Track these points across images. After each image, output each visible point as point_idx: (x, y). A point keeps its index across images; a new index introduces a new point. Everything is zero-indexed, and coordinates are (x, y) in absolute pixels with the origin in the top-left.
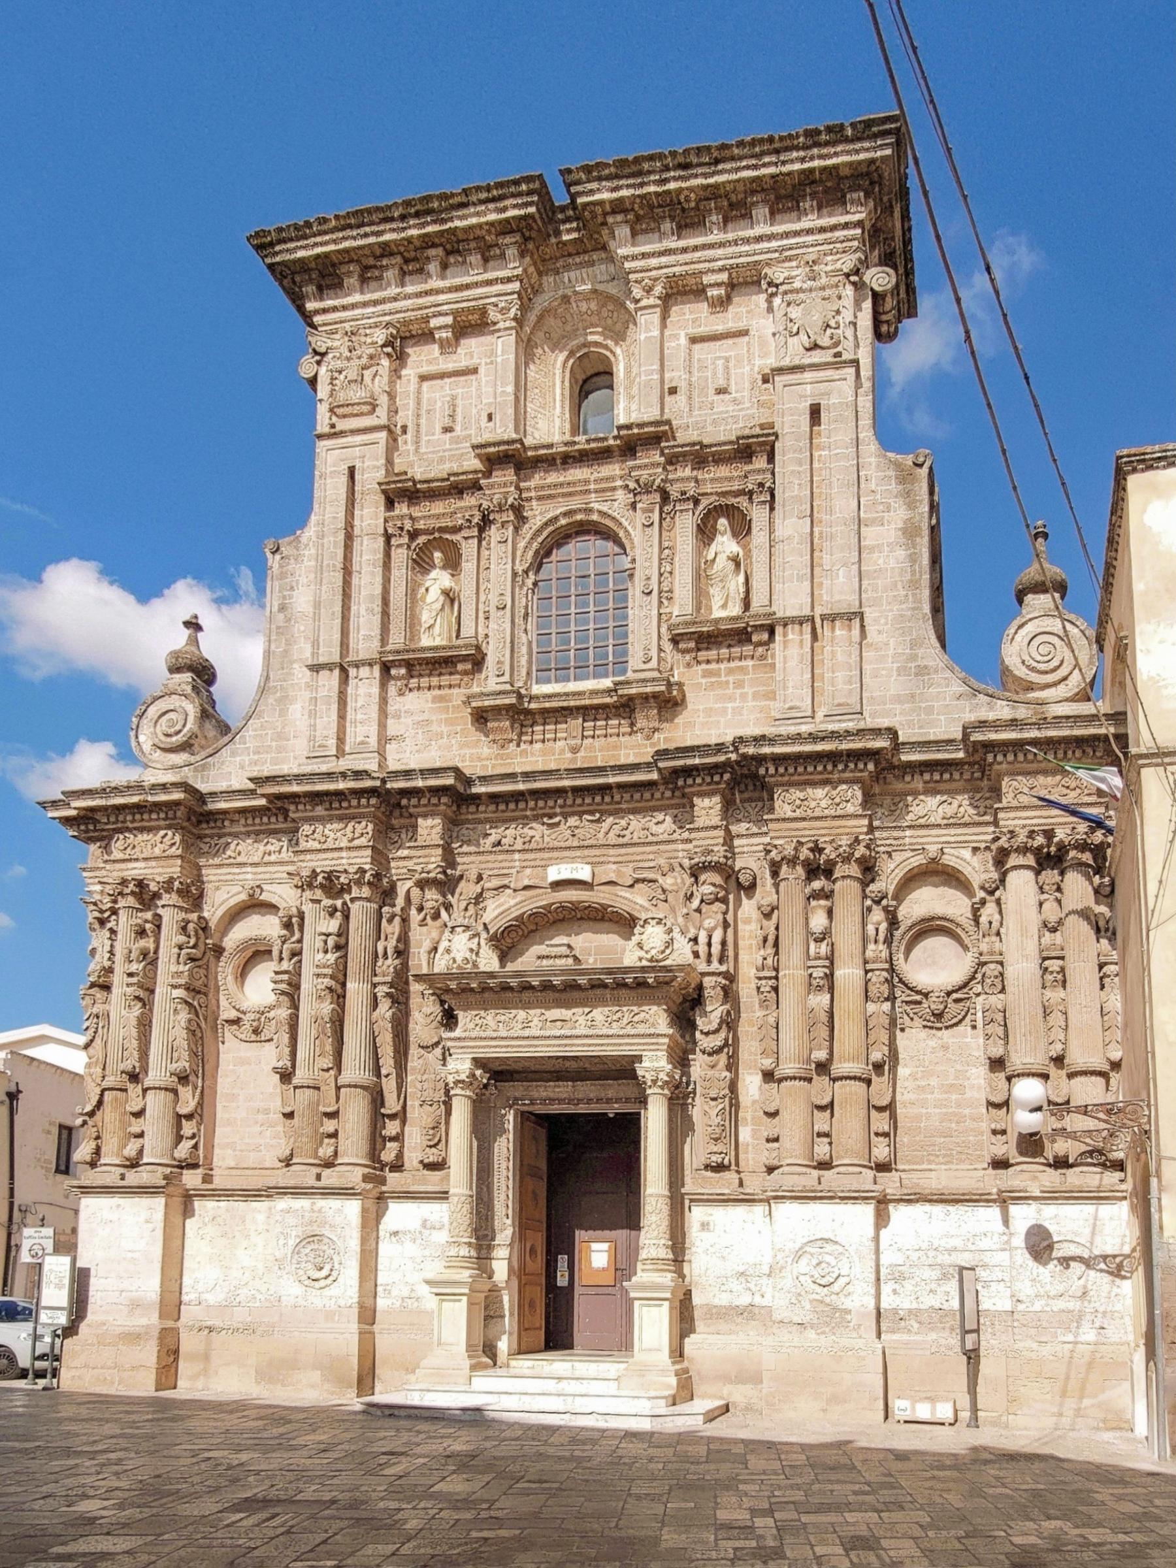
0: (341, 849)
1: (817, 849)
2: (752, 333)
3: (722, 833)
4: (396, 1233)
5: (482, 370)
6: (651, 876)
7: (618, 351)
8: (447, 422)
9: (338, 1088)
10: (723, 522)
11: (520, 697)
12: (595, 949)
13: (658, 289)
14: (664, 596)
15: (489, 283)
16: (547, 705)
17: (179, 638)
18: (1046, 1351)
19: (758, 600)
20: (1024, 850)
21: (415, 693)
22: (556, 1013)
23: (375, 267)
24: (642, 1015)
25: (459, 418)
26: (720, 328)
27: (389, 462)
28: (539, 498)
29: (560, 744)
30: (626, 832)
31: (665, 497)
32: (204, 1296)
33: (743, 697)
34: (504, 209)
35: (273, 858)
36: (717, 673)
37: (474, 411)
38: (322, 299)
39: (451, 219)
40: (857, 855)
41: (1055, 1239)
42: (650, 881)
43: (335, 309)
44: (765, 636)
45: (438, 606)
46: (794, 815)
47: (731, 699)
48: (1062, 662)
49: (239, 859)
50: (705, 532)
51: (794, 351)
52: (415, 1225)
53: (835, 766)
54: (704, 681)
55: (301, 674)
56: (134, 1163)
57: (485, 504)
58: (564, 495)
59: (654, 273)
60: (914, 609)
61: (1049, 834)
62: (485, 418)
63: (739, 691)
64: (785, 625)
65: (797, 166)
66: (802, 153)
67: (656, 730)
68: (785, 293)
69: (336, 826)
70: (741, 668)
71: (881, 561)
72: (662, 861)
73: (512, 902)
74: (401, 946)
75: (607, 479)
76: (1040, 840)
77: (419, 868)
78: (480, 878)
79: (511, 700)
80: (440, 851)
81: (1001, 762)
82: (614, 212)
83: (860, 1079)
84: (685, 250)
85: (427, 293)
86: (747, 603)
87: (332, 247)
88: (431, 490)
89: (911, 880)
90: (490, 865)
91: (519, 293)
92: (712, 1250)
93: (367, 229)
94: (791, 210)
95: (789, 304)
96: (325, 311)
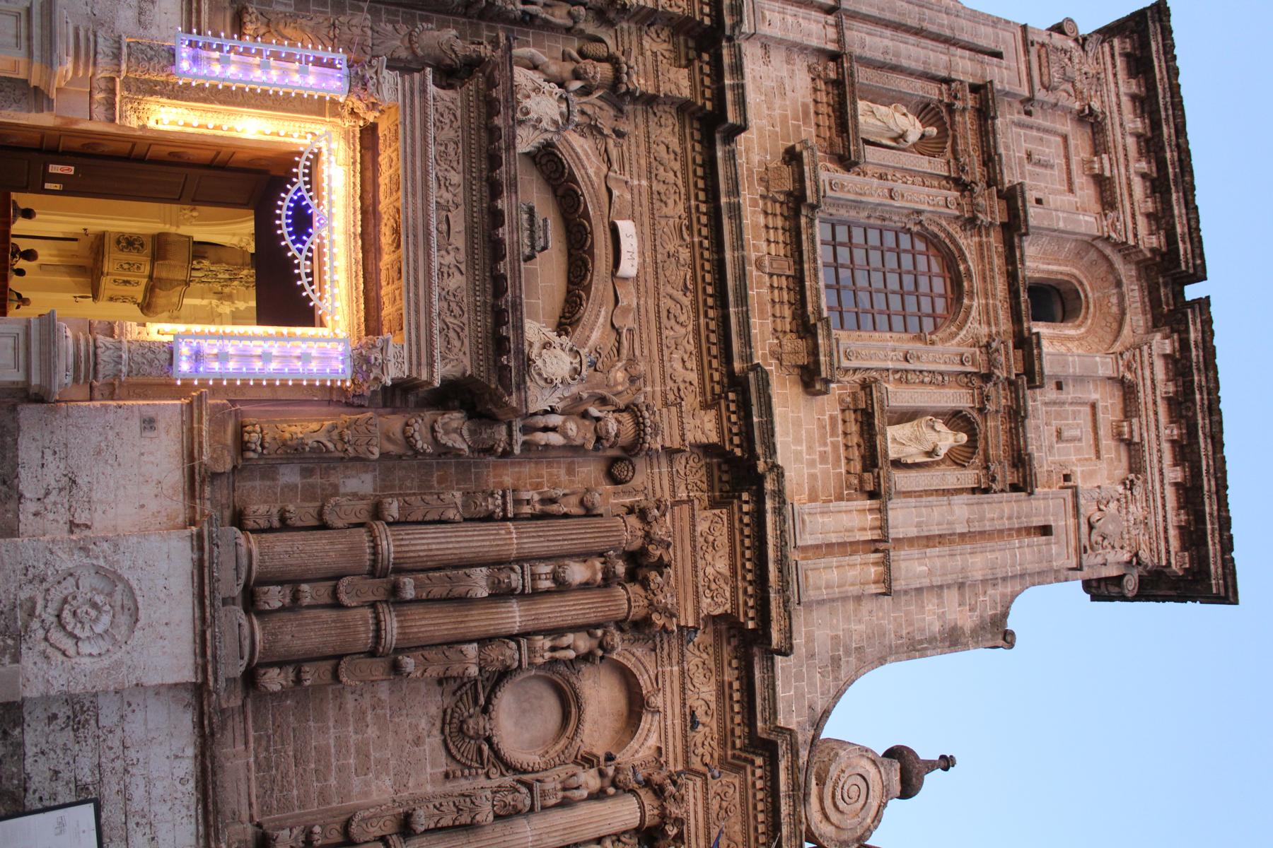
1: (660, 566)
2: (1098, 462)
3: (676, 446)
5: (1070, 197)
6: (624, 351)
7: (1083, 330)
8: (1035, 157)
11: (813, 207)
12: (544, 279)
13: (1129, 376)
14: (903, 377)
16: (804, 237)
19: (902, 480)
20: (663, 816)
21: (809, 84)
22: (458, 225)
23: (1143, 112)
24: (457, 343)
25: (1038, 170)
26: (1102, 433)
27: (1007, 94)
29: (764, 245)
30: (673, 321)
31: (986, 378)
33: (812, 463)
36: (834, 433)
37: (1043, 185)
38: (1121, 54)
39: (1177, 192)
40: (655, 617)
42: (618, 351)
43: (1114, 66)
44: (869, 487)
45: (892, 126)
46: (698, 534)
47: (810, 448)
48: (842, 812)
50: (956, 419)
51: (1088, 508)
53: (750, 583)
54: (827, 417)
57: (977, 189)
58: (984, 270)
59: (1139, 372)
60: (890, 647)
62: (1039, 195)
63: (817, 457)
64: (880, 510)
65: (1207, 509)
66: (1215, 513)
67: (780, 360)
68: (1126, 497)
70: (838, 460)
71: (930, 607)
72: (642, 367)
73: (591, 171)
74: (537, 22)
75: (996, 318)
76: (672, 831)
77: (632, 63)
78: (620, 134)
79: (811, 198)
80: (651, 91)
82: (1181, 340)
84: (1155, 403)
86: (897, 464)
87: (1158, 76)
88: (987, 133)
90: (633, 149)
91: (1126, 243)
92: (111, 435)
93: (1170, 112)
95: (1118, 500)
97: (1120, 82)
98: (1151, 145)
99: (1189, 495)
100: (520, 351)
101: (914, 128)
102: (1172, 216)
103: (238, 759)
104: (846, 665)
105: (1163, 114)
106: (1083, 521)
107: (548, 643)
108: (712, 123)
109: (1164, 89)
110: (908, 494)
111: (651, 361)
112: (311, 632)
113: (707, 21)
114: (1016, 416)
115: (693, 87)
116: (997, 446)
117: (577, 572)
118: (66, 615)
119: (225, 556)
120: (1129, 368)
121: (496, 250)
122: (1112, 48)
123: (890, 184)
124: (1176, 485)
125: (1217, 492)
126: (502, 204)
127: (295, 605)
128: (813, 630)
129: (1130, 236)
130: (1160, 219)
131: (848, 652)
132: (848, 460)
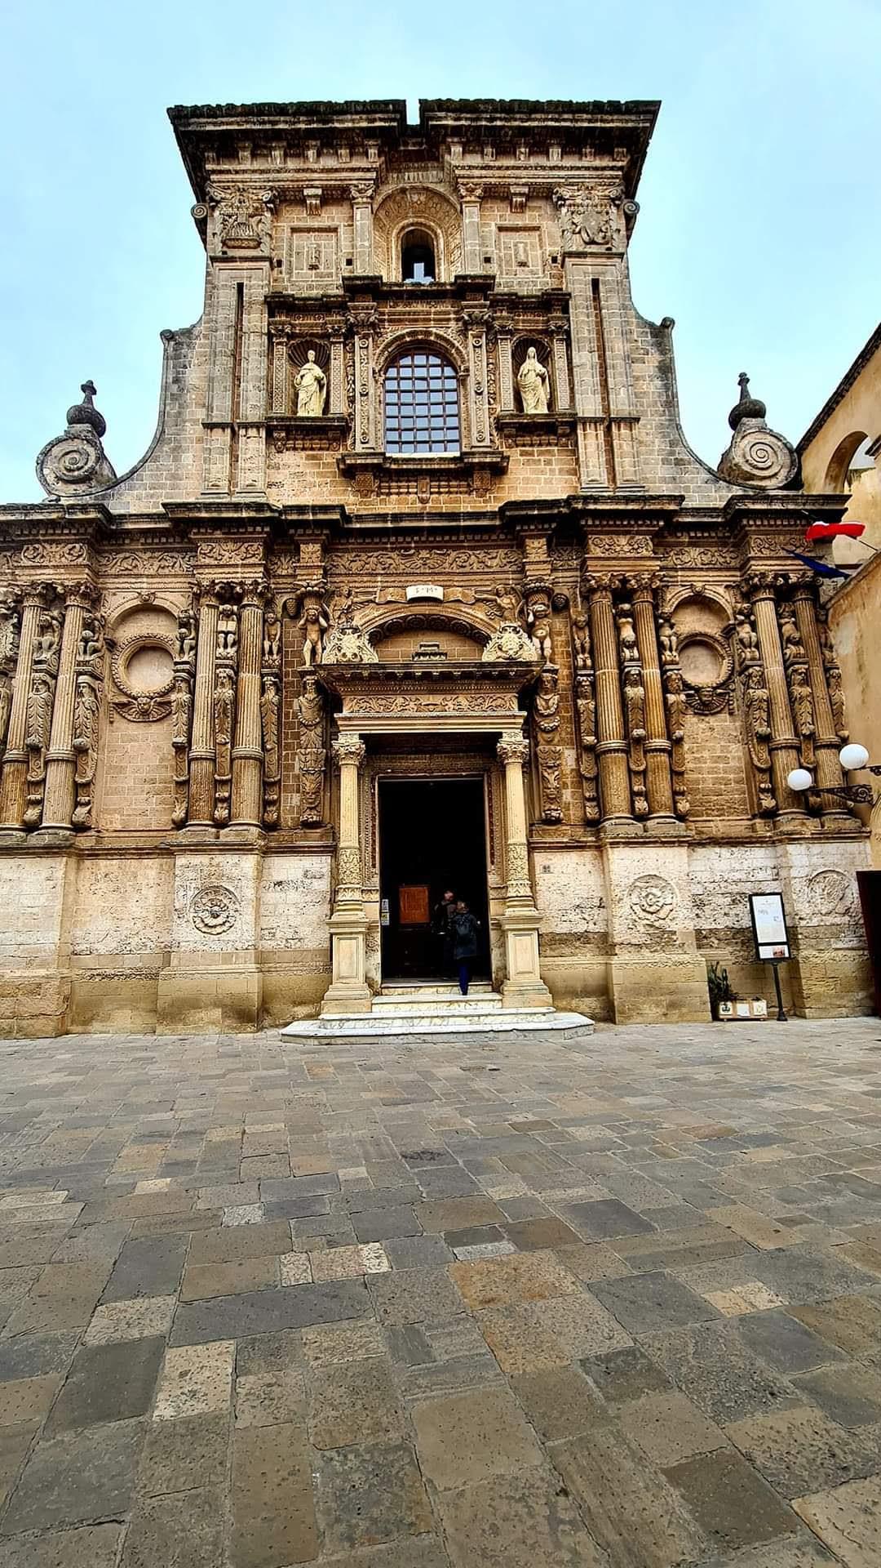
0: (236, 566)
1: (625, 581)
4: (280, 883)
5: (341, 230)
9: (232, 760)
10: (532, 350)
13: (479, 192)
14: (494, 397)
15: (353, 170)
17: (79, 398)
18: (826, 955)
19: (562, 404)
20: (253, 592)
22: (432, 699)
23: (265, 147)
25: (323, 260)
26: (520, 223)
28: (390, 321)
31: (490, 327)
32: (97, 946)
34: (374, 120)
35: (166, 571)
39: (332, 121)
41: (88, 863)
43: (228, 172)
49: (135, 571)
50: (519, 358)
51: (576, 244)
52: (300, 874)
55: (193, 430)
56: (30, 827)
58: (410, 321)
61: (786, 577)
62: (343, 264)
64: (584, 424)
69: (231, 546)
78: (349, 594)
81: (750, 524)
82: (453, 135)
83: (791, 747)
84: (499, 168)
85: (304, 171)
86: (326, 409)
87: (236, 127)
89: (684, 604)
94: (574, 153)
96: (221, 172)
97: (238, 168)
98: (295, 145)
99: (573, 142)
100: (508, 665)
101: (311, 371)
102: (353, 129)
103: (718, 826)
104: (679, 455)
105: (268, 127)
106: (589, 249)
107: (668, 653)
108: (336, 532)
109: (247, 122)
110: (572, 399)
111: (494, 580)
112: (662, 787)
113: (267, 529)
114: (514, 303)
115: (314, 542)
116: (537, 322)
117: (628, 633)
118: (651, 909)
119: (622, 831)
120: (471, 191)
121: (446, 677)
122: (214, 172)
123: (358, 395)
124: (564, 153)
125: (573, 113)
126: (418, 672)
127: (646, 795)
128: (658, 480)
129: (369, 175)
130: (354, 142)
131: (672, 453)
132: (549, 444)
